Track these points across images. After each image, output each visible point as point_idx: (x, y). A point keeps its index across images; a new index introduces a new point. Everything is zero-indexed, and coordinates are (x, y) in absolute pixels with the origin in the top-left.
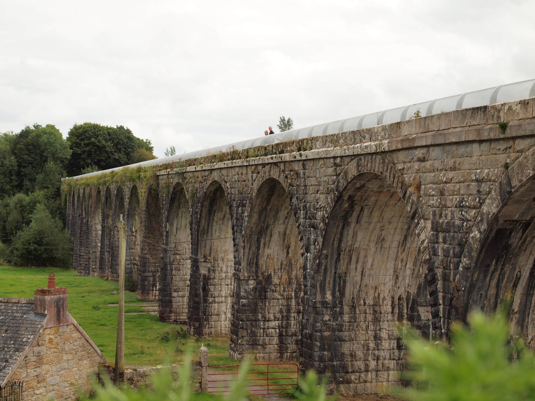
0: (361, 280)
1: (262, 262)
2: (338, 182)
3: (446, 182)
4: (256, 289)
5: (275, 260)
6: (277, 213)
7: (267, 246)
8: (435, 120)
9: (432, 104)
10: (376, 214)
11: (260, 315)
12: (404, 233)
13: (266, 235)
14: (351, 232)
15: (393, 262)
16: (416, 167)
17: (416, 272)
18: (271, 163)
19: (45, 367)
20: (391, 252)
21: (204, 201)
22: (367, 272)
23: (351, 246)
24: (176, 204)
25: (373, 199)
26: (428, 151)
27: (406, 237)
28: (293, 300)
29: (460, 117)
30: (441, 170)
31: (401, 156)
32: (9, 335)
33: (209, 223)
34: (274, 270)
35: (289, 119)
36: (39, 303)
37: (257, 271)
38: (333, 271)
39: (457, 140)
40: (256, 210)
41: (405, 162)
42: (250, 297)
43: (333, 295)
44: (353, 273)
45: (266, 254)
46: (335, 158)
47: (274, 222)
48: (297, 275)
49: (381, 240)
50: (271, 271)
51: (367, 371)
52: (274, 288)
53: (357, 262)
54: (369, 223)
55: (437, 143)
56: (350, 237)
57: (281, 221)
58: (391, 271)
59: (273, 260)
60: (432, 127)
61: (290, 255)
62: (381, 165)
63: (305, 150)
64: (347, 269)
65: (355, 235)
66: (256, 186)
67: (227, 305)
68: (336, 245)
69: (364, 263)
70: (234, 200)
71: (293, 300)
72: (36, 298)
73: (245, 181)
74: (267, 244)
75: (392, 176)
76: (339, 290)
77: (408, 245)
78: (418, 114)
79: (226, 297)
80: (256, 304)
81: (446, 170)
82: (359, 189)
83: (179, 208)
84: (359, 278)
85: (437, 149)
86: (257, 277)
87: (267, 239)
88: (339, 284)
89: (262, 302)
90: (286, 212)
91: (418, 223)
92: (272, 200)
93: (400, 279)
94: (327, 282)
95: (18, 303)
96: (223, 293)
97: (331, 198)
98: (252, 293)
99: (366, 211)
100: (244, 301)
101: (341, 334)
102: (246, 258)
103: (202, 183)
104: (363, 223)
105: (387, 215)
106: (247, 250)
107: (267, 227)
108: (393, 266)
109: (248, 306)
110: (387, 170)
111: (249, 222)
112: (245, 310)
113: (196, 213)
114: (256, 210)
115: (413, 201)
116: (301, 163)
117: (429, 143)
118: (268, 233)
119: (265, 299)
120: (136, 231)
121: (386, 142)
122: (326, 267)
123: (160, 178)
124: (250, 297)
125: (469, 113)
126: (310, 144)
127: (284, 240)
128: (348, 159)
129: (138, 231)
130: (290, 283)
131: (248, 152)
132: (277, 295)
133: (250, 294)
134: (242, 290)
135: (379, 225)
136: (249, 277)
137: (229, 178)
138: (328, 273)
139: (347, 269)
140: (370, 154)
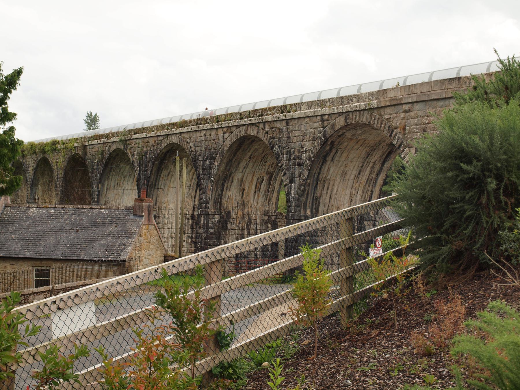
0: (330, 201)
1: (224, 201)
2: (325, 131)
4: (220, 221)
5: (234, 200)
6: (238, 164)
7: (228, 189)
8: (418, 86)
10: (345, 155)
11: (222, 241)
12: (359, 169)
13: (229, 180)
15: (350, 190)
16: (402, 116)
17: (363, 197)
18: (248, 124)
20: (349, 183)
21: (155, 160)
22: (333, 195)
23: (325, 178)
24: (109, 167)
25: (345, 144)
26: (413, 106)
27: (360, 172)
28: (246, 230)
33: (156, 179)
34: (233, 208)
35: (96, 115)
36: (137, 207)
37: (220, 208)
38: (312, 195)
39: (439, 97)
40: (225, 161)
41: (391, 114)
42: (216, 228)
45: (227, 196)
47: (236, 170)
49: (344, 174)
50: (230, 208)
52: (232, 221)
53: (328, 189)
54: (339, 161)
55: (422, 100)
56: (326, 170)
57: (241, 171)
58: (348, 196)
59: (232, 200)
60: (415, 91)
61: (244, 196)
62: (369, 117)
63: (289, 112)
64: (321, 194)
65: (329, 169)
66: (228, 143)
67: (168, 245)
68: (316, 177)
69: (332, 190)
70: (200, 155)
71: (246, 230)
72: (135, 205)
73: (214, 140)
74: (229, 187)
75: (379, 123)
76: (315, 208)
77: (360, 178)
79: (167, 238)
80: (220, 233)
82: (339, 136)
83: (111, 171)
84: (328, 200)
85: (420, 104)
86: (221, 212)
87: (229, 184)
88: (316, 204)
90: (245, 163)
91: (403, 151)
92: (238, 153)
94: (308, 202)
95: (118, 209)
97: (318, 143)
98: (217, 224)
99: (339, 152)
100: (212, 230)
101: (317, 238)
102: (213, 198)
105: (351, 156)
106: (214, 192)
108: (349, 193)
109: (214, 234)
111: (218, 170)
113: (147, 171)
115: (399, 138)
116: (284, 122)
117: (415, 100)
119: (226, 229)
120: (38, 199)
122: (308, 192)
123: (88, 147)
124: (216, 228)
125: (447, 82)
126: (294, 108)
127: (241, 185)
130: (243, 218)
132: (234, 226)
133: (216, 225)
135: (345, 163)
136: (215, 212)
137: (192, 140)
139: (321, 194)
140: (359, 110)
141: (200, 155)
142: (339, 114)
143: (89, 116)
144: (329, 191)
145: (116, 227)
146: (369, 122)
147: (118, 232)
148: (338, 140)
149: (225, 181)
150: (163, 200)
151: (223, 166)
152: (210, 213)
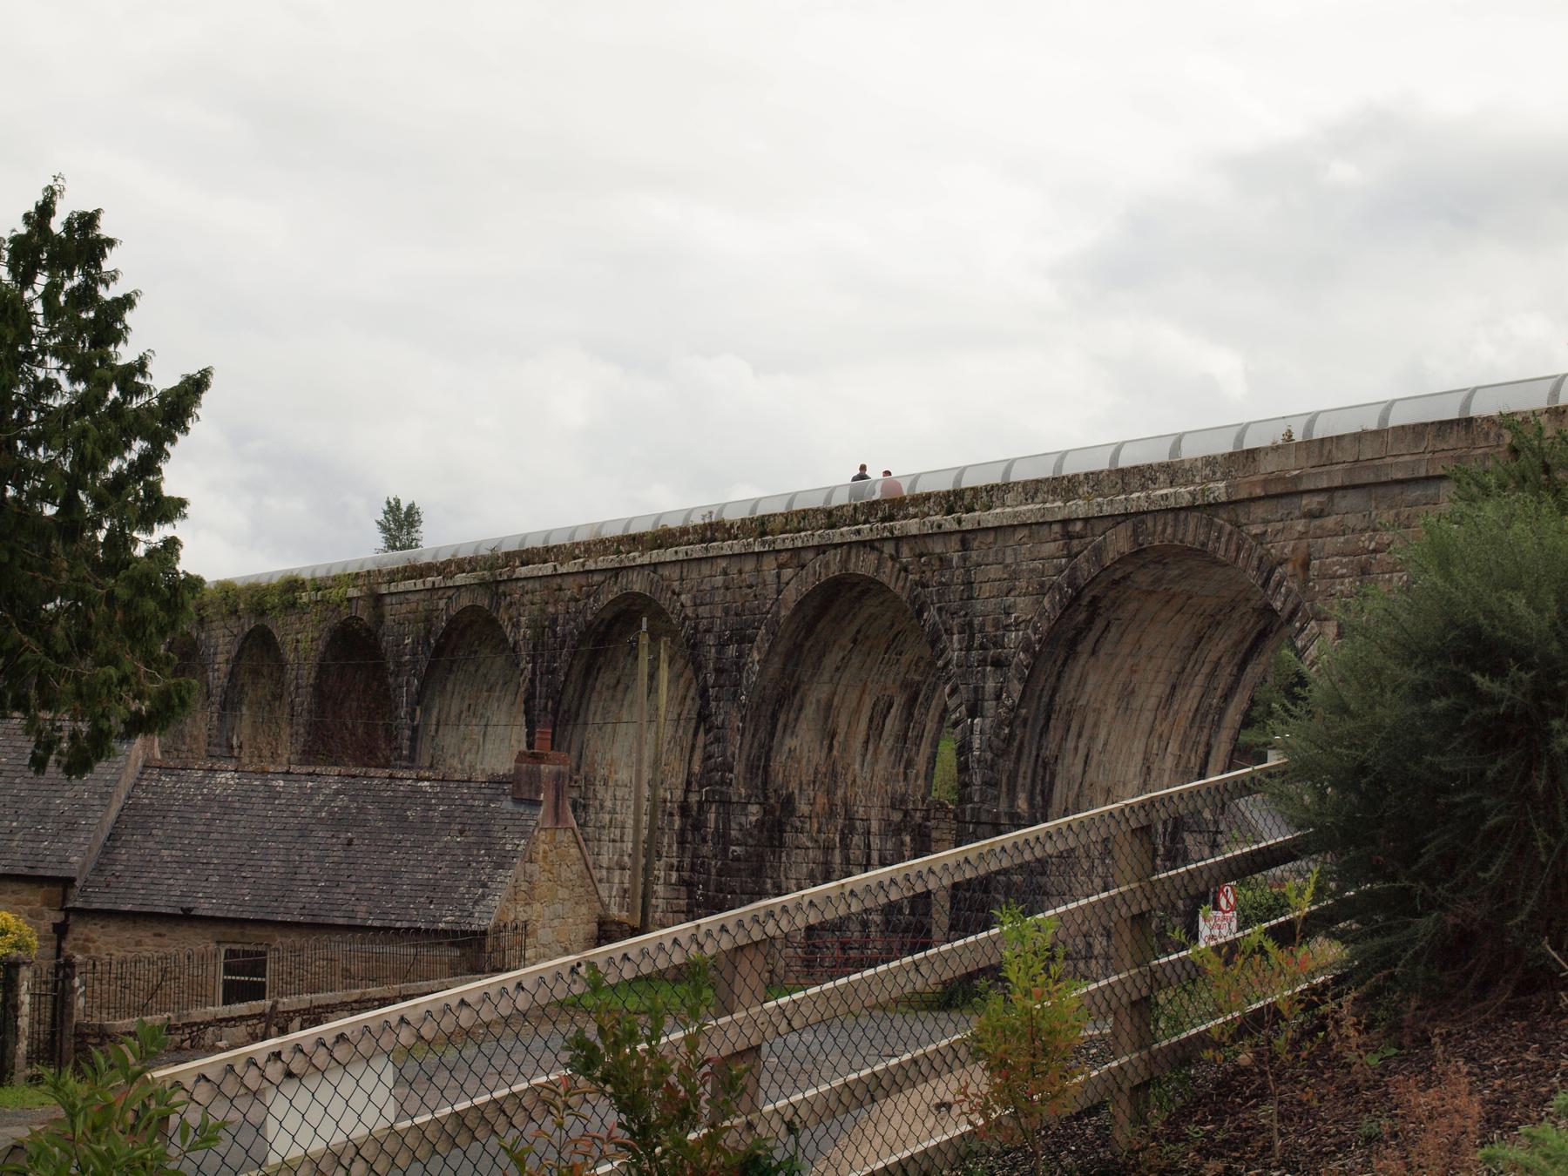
0: (1084, 772)
1: (775, 765)
2: (1074, 569)
3: (1375, 551)
8: (1345, 443)
9: (1313, 418)
10: (1129, 638)
14: (1077, 672)
15: (1144, 740)
17: (1183, 762)
19: (537, 906)
22: (1095, 757)
25: (1132, 606)
26: (1331, 499)
27: (1174, 687)
28: (837, 852)
29: (1410, 436)
30: (1363, 531)
31: (1259, 511)
32: (472, 839)
34: (801, 784)
37: (765, 789)
38: (1034, 753)
39: (1409, 476)
40: (780, 648)
42: (750, 841)
43: (1031, 800)
44: (1068, 760)
45: (786, 749)
46: (1065, 522)
47: (813, 675)
48: (846, 797)
49: (1128, 693)
50: (794, 786)
51: (1087, 958)
53: (1079, 736)
55: (1357, 481)
57: (826, 677)
58: (1139, 758)
61: (835, 752)
66: (791, 595)
67: (611, 888)
68: (1045, 699)
69: (1092, 738)
70: (708, 631)
71: (837, 852)
72: (517, 769)
76: (1042, 792)
78: (1289, 435)
79: (609, 869)
80: (761, 857)
81: (1374, 530)
83: (450, 671)
84: (1078, 769)
86: (766, 797)
87: (792, 715)
88: (1043, 778)
89: (774, 853)
91: (1302, 629)
93: (1154, 774)
95: (469, 781)
96: (604, 860)
97: (1052, 602)
98: (755, 832)
99: (1113, 629)
103: (577, 600)
104: (1102, 653)
106: (748, 736)
107: (796, 688)
108: (1142, 748)
109: (746, 861)
110: (1218, 538)
111: (761, 674)
112: (739, 870)
113: (554, 671)
114: (780, 648)
115: (1289, 591)
118: (796, 702)
120: (240, 747)
121: (1222, 485)
122: (1022, 743)
124: (750, 841)
127: (826, 719)
128: (1109, 523)
129: (246, 748)
131: (763, 524)
133: (751, 835)
134: (733, 825)
136: (749, 797)
138: (1025, 757)
141: (708, 631)
142: (1117, 519)
143: (393, 509)
144: (1082, 744)
145: (461, 832)
146: (1203, 544)
147: (467, 848)
148: (1112, 594)
149: (781, 706)
150: (598, 757)
151: (777, 662)
152: (735, 799)
